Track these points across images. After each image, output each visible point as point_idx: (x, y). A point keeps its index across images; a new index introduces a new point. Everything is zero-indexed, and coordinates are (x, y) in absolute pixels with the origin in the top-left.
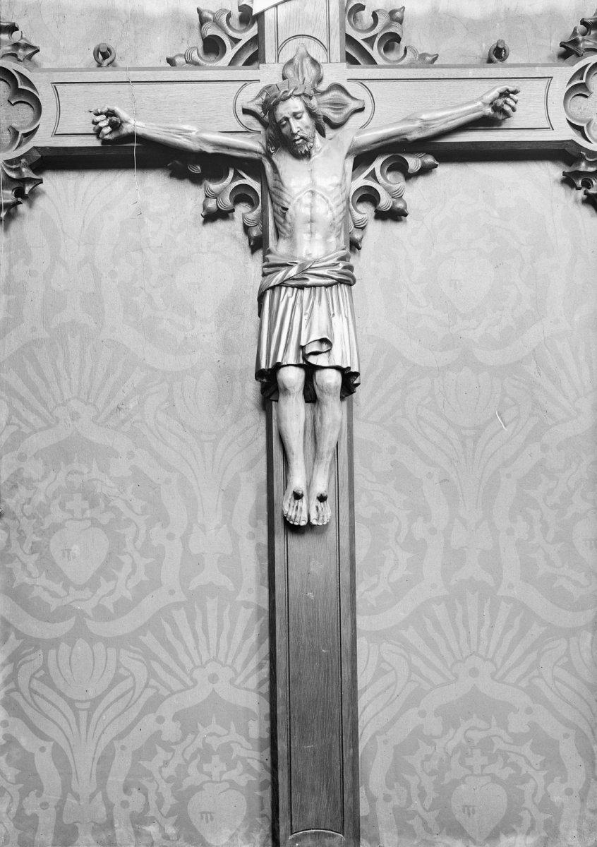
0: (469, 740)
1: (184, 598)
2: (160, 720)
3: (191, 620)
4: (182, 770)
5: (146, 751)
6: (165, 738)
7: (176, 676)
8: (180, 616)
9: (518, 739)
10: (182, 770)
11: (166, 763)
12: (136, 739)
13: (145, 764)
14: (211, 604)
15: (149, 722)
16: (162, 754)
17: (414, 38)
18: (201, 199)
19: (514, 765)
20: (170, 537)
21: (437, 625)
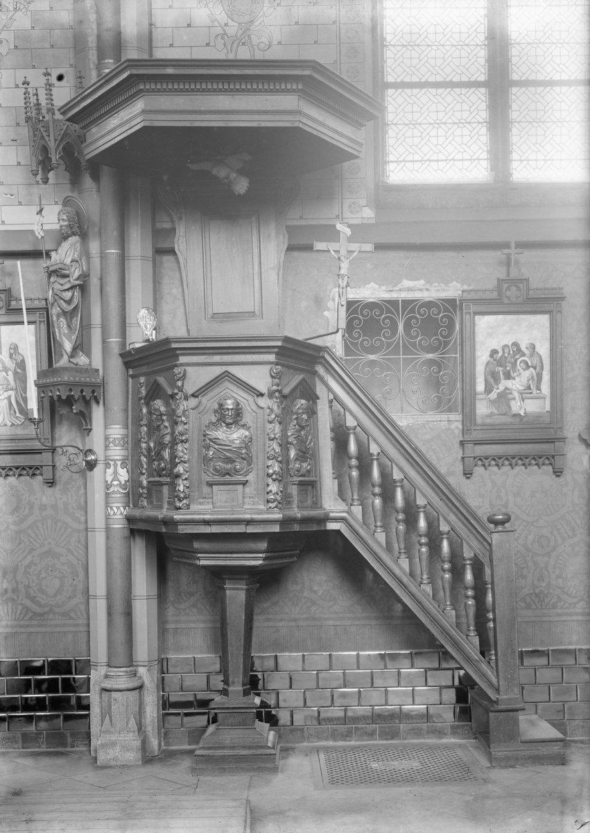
0: (48, 565)
1: (41, 518)
2: (565, 546)
3: (43, 525)
4: (40, 573)
5: (29, 566)
6: (35, 562)
7: (37, 542)
8: (39, 524)
9: (63, 564)
10: (40, 573)
11: (35, 570)
12: (27, 562)
13: (28, 570)
14: (49, 521)
15: (29, 558)
16: (33, 567)
17: (78, 75)
18: (185, 387)
19: (62, 573)
20: (529, 572)
21: (47, 527)
